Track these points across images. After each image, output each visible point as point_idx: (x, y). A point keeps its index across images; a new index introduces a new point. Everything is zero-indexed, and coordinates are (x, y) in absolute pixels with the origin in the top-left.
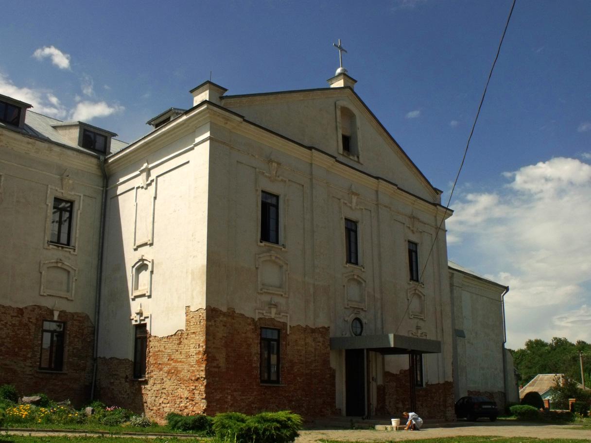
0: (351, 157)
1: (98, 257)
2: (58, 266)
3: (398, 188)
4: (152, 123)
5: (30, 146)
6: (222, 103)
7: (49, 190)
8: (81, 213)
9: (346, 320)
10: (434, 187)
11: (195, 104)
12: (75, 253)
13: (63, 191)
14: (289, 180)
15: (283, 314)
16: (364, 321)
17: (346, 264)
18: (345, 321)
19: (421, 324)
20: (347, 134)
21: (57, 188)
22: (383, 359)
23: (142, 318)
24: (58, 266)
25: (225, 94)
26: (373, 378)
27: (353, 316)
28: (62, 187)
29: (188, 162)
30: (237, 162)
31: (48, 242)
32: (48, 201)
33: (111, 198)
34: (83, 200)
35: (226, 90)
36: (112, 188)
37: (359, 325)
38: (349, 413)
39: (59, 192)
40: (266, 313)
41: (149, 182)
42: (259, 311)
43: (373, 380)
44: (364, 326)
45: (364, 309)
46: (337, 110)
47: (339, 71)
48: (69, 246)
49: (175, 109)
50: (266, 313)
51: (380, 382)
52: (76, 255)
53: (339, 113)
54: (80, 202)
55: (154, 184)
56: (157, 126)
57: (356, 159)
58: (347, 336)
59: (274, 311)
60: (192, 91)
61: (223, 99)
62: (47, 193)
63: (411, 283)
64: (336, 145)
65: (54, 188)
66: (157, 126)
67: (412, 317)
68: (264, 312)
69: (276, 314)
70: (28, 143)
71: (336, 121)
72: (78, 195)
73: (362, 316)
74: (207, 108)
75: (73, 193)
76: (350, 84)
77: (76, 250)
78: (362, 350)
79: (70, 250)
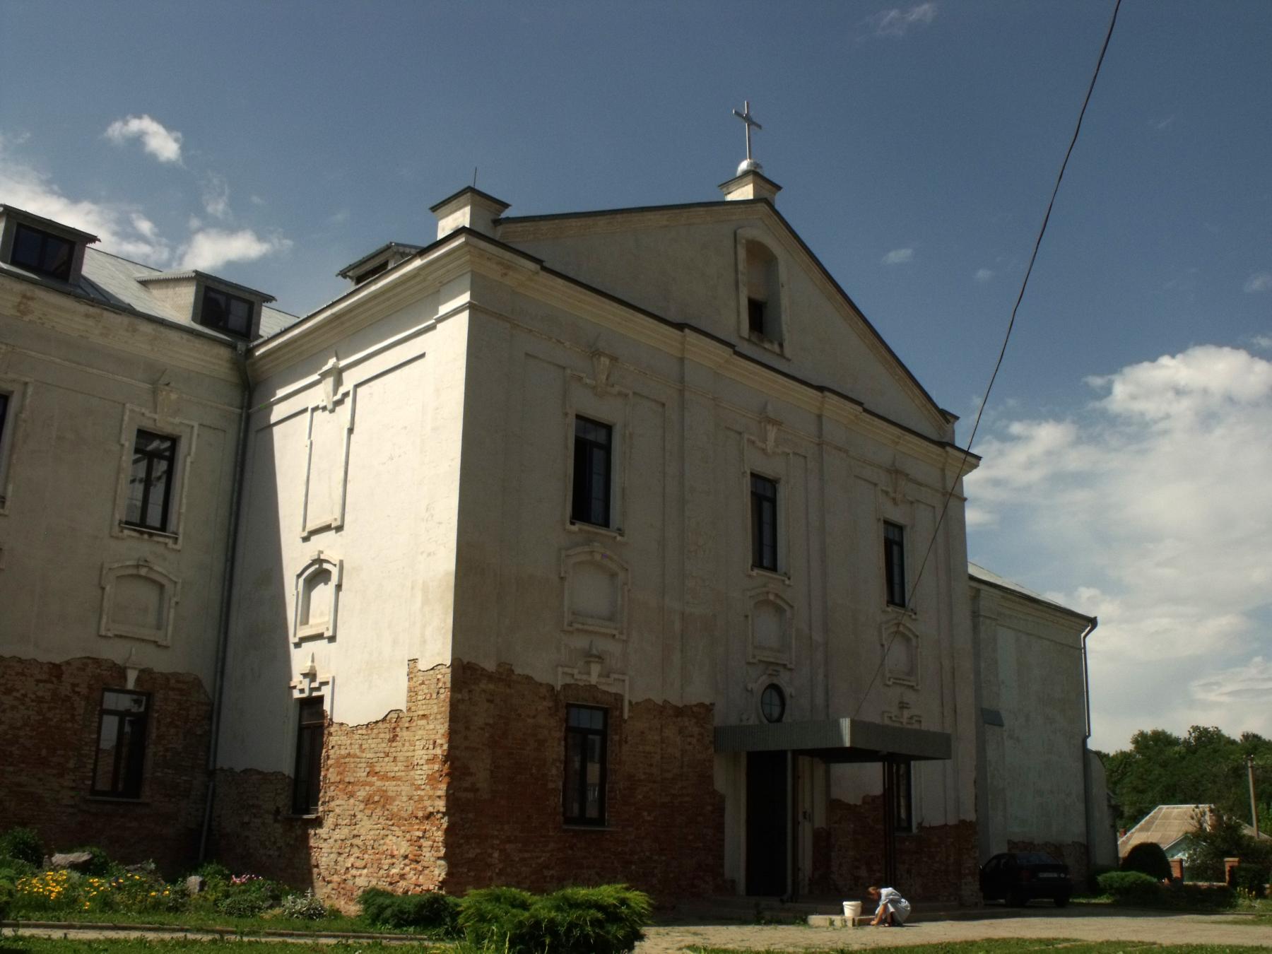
0: (767, 346)
1: (226, 555)
2: (140, 574)
3: (865, 410)
4: (350, 274)
5: (90, 322)
6: (498, 234)
7: (128, 413)
8: (192, 463)
9: (749, 688)
10: (941, 406)
11: (441, 235)
12: (178, 547)
13: (156, 416)
14: (635, 393)
15: (616, 676)
16: (788, 690)
17: (752, 570)
18: (747, 690)
19: (910, 697)
20: (759, 297)
21: (143, 410)
22: (828, 772)
23: (315, 685)
24: (140, 574)
25: (506, 214)
26: (805, 813)
27: (764, 681)
28: (156, 407)
29: (422, 356)
30: (527, 354)
31: (120, 522)
32: (123, 437)
33: (258, 431)
34: (198, 435)
35: (506, 206)
36: (260, 410)
37: (776, 700)
38: (752, 890)
39: (149, 418)
40: (579, 673)
41: (339, 396)
42: (566, 670)
43: (805, 817)
44: (788, 701)
45: (789, 666)
46: (739, 247)
47: (744, 165)
48: (165, 531)
49: (397, 245)
50: (579, 673)
51: (820, 820)
52: (179, 551)
53: (742, 253)
54: (191, 439)
55: (349, 401)
56: (359, 280)
57: (776, 348)
58: (751, 722)
59: (595, 669)
60: (434, 209)
61: (501, 224)
62: (122, 420)
63: (889, 609)
64: (735, 320)
65: (137, 409)
66: (359, 280)
67: (890, 683)
68: (575, 671)
69: (600, 676)
70: (87, 316)
71: (736, 271)
72: (188, 425)
73: (783, 680)
74: (466, 243)
75: (177, 420)
76: (766, 194)
77: (180, 541)
78: (784, 753)
79: (167, 540)
